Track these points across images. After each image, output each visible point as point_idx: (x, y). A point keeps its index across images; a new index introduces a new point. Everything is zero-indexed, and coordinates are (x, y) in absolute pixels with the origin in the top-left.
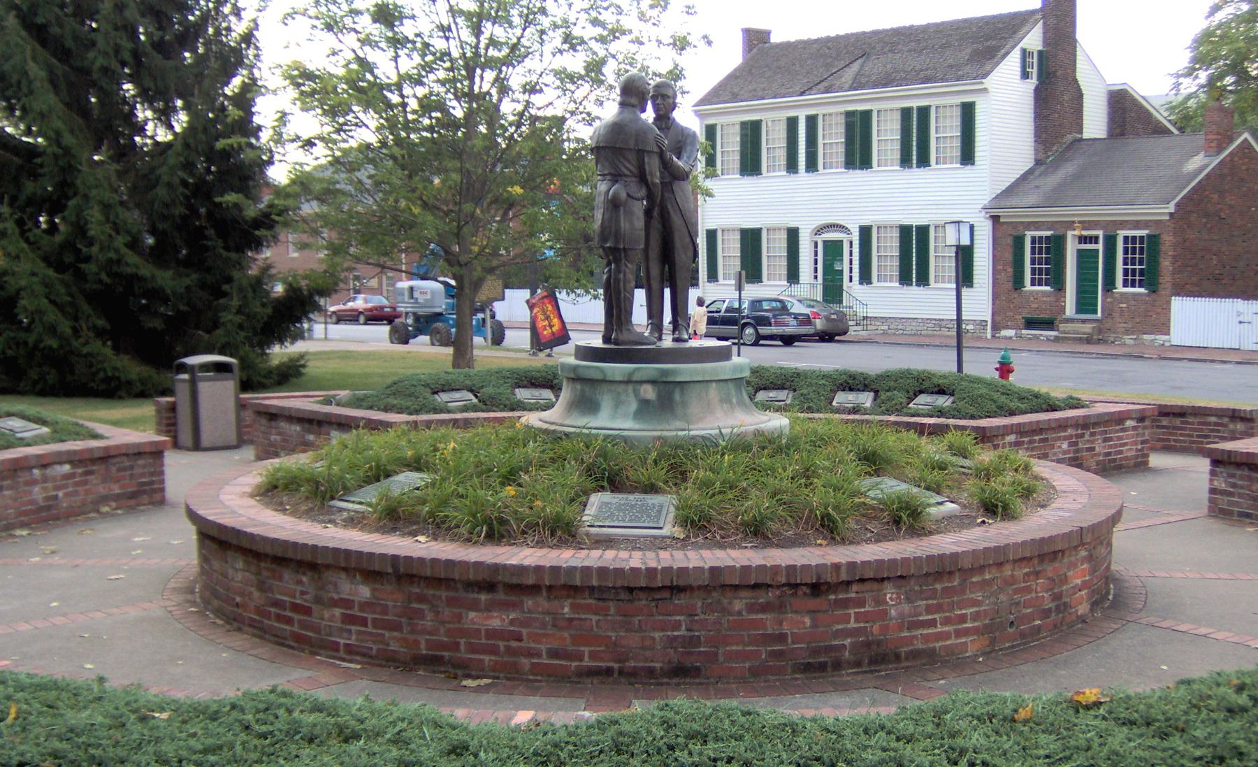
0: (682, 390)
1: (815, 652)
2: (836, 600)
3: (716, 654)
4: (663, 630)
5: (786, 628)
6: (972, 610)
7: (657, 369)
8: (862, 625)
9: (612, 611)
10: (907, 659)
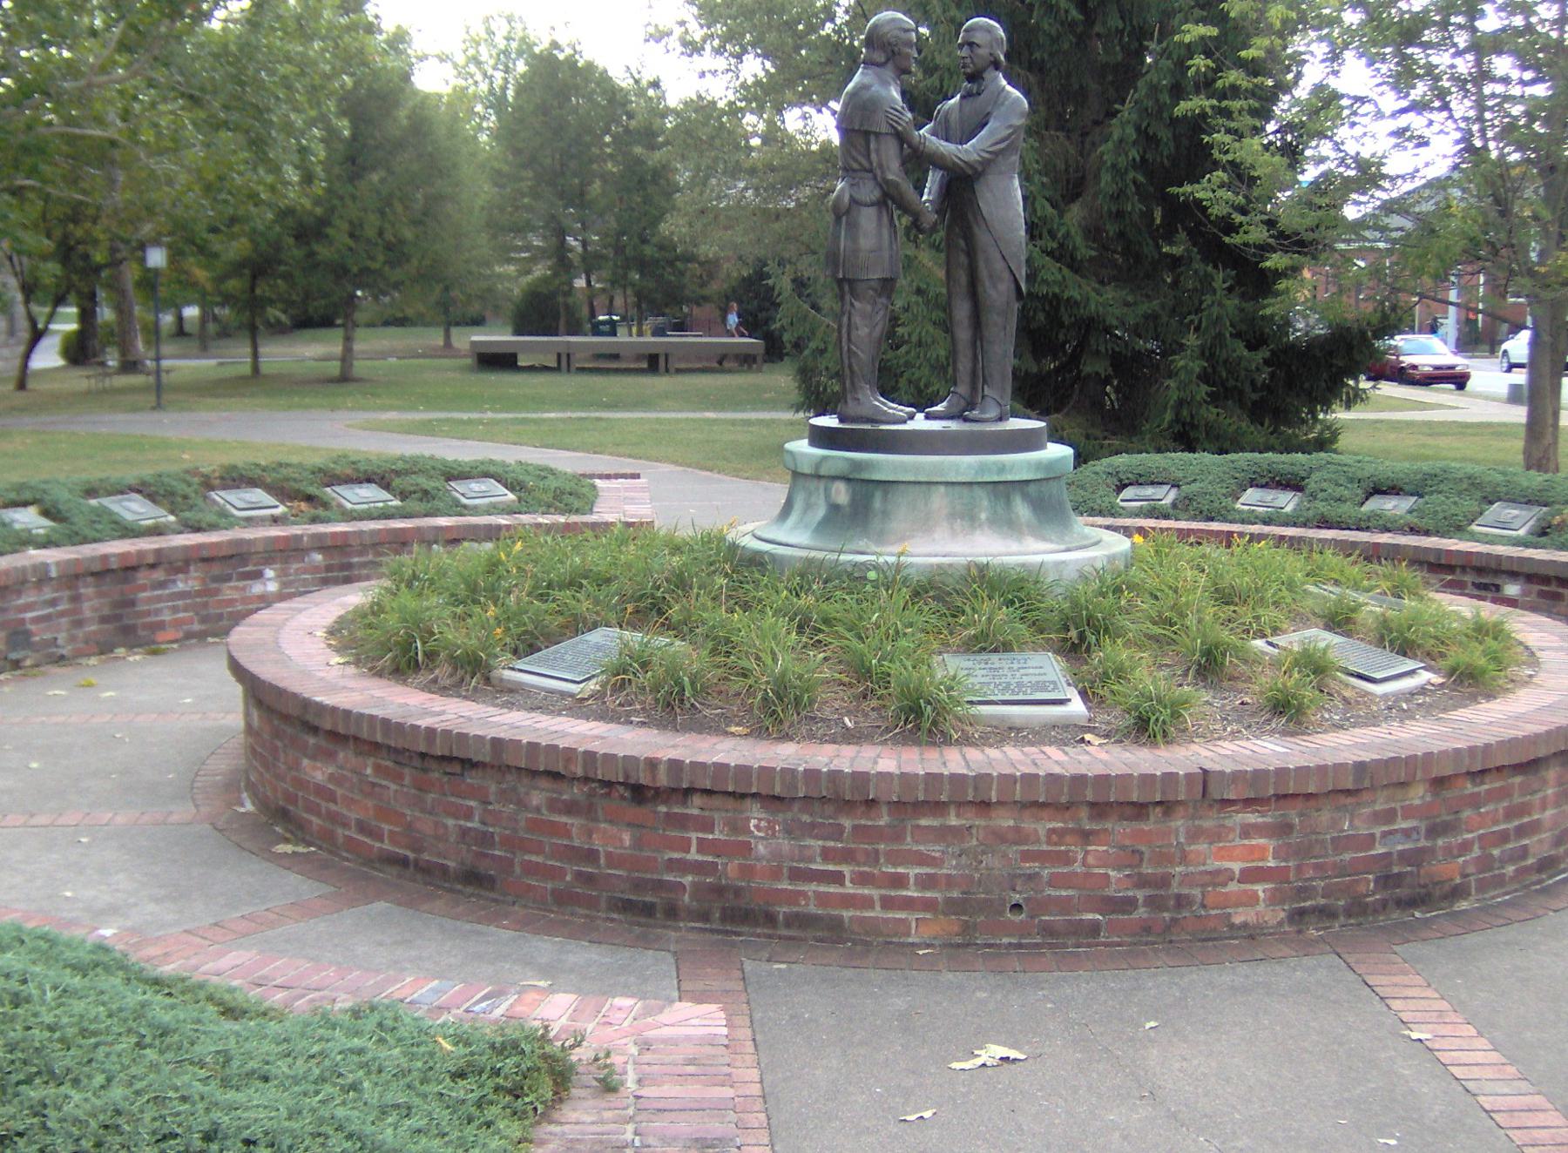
0: (886, 493)
1: (638, 885)
2: (667, 814)
3: (511, 863)
4: (457, 818)
5: (597, 843)
6: (918, 870)
7: (847, 459)
8: (710, 859)
9: (407, 781)
10: (788, 925)
